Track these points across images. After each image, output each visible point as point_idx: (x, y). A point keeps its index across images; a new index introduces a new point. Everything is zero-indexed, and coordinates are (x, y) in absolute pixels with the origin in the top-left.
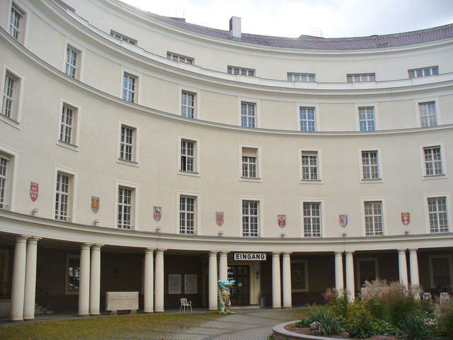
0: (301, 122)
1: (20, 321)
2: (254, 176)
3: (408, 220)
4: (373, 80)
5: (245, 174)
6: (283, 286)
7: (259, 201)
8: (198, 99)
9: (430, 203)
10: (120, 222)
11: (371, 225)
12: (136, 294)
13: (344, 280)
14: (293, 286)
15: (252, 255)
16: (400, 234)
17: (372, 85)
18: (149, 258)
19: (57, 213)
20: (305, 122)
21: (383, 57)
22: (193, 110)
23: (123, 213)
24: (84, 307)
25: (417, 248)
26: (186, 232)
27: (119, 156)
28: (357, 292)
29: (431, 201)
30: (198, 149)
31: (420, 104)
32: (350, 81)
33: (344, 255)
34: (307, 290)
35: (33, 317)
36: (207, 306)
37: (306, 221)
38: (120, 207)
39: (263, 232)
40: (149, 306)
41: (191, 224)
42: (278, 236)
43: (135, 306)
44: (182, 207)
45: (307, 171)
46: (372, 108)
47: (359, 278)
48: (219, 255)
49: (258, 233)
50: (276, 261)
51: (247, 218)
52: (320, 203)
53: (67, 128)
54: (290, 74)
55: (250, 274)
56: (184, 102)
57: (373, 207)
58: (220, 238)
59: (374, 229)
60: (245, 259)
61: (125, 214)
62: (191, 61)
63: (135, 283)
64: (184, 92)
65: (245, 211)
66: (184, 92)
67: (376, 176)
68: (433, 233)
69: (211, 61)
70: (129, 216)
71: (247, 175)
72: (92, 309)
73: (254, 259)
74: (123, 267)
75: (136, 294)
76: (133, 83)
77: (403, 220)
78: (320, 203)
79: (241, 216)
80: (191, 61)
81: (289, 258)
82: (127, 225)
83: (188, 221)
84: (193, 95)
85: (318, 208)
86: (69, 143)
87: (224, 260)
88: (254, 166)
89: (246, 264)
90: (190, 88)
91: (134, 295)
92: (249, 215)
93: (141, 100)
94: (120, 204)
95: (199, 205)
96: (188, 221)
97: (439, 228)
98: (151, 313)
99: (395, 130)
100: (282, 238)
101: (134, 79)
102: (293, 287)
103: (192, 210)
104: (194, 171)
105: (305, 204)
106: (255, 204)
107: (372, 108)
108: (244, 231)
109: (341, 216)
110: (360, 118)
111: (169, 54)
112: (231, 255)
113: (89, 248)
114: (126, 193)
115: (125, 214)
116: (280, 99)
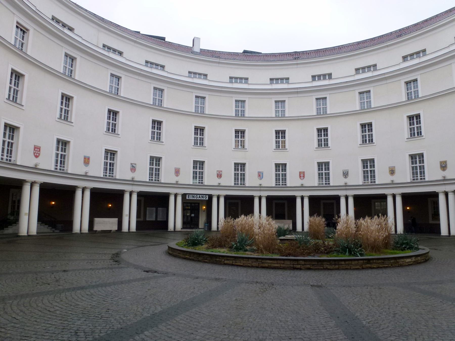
0: (195, 106)
1: (24, 236)
3: (304, 176)
4: (246, 83)
5: (153, 138)
6: (175, 218)
7: (161, 158)
10: (57, 166)
11: (279, 179)
12: (116, 220)
14: (138, 216)
15: (198, 196)
18: (79, 193)
19: (2, 155)
22: (118, 89)
23: (59, 159)
24: (76, 228)
25: (266, 195)
27: (58, 116)
30: (121, 118)
32: (231, 82)
33: (260, 198)
35: (35, 234)
38: (57, 154)
39: (247, 183)
40: (125, 228)
41: (112, 170)
43: (115, 228)
44: (106, 158)
45: (197, 140)
46: (244, 101)
48: (131, 193)
49: (159, 179)
50: (215, 200)
51: (153, 168)
53: (14, 90)
56: (111, 82)
57: (323, 166)
58: (177, 185)
59: (281, 181)
61: (61, 160)
62: (121, 53)
63: (117, 213)
65: (151, 164)
67: (326, 145)
69: (135, 56)
70: (64, 161)
72: (30, 230)
74: (106, 201)
75: (116, 220)
76: (72, 62)
77: (300, 177)
78: (204, 161)
80: (121, 53)
81: (181, 197)
82: (62, 168)
83: (110, 167)
84: (119, 78)
85: (203, 165)
86: (16, 102)
87: (179, 199)
88: (160, 133)
89: (198, 202)
90: (117, 73)
91: (115, 220)
92: (154, 167)
93: (77, 76)
94: (57, 152)
96: (110, 167)
97: (281, 183)
98: (126, 232)
99: (298, 117)
101: (73, 59)
102: (439, 225)
103: (113, 160)
104: (116, 132)
105: (235, 164)
106: (159, 160)
107: (244, 101)
108: (150, 177)
109: (259, 173)
110: (276, 108)
111: (104, 46)
112: (184, 196)
113: (30, 184)
114: (63, 144)
115: (61, 160)
116: (388, 81)
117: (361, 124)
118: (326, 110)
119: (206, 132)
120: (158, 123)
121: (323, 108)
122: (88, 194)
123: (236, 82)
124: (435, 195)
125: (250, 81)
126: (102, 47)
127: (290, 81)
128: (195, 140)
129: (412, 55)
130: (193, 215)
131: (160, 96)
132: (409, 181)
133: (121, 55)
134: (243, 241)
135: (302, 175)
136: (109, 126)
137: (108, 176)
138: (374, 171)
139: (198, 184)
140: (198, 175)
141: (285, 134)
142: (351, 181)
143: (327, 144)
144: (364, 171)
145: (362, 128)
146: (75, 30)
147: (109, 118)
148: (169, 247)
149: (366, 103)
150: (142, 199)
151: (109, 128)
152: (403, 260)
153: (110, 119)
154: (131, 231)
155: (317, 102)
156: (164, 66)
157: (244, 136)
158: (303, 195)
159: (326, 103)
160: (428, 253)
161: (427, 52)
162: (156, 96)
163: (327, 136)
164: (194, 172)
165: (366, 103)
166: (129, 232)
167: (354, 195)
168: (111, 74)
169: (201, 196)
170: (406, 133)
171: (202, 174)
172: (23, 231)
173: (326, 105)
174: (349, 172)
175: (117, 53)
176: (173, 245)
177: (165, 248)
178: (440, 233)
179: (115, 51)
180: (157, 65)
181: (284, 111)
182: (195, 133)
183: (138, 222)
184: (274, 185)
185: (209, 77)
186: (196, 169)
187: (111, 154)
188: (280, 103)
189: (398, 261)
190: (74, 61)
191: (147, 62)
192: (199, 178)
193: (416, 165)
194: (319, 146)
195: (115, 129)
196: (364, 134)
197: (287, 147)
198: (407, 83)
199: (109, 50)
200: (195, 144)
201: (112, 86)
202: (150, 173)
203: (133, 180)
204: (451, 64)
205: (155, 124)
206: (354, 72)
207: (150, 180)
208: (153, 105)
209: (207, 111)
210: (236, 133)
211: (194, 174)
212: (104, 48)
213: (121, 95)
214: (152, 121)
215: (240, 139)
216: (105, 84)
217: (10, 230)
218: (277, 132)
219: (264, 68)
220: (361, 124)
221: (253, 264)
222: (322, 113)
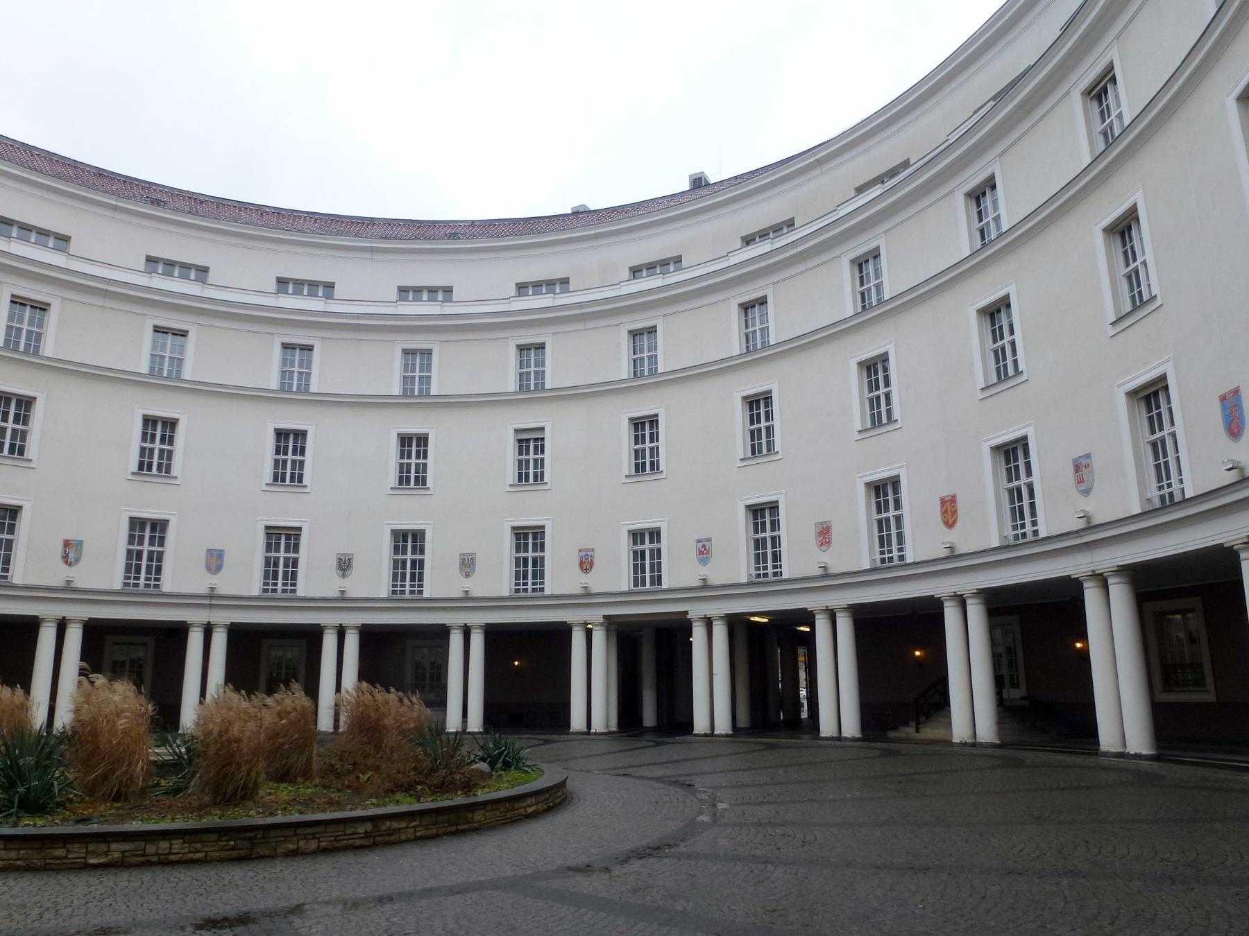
9: (132, 528)
11: (526, 573)
17: (57, 259)
21: (110, 213)
24: (700, 723)
29: (137, 524)
31: (157, 330)
33: (62, 626)
34: (1210, 697)
36: (688, 726)
37: (270, 563)
39: (303, 588)
42: (202, 589)
46: (309, 348)
48: (708, 623)
52: (21, 507)
57: (283, 539)
68: (395, 597)
83: (766, 550)
96: (766, 550)
107: (309, 348)
118: (429, 383)
119: (38, 413)
121: (420, 377)
122: (845, 625)
125: (212, 277)
127: (338, 293)
132: (506, 593)
134: (291, 754)
135: (215, 561)
137: (770, 574)
138: (422, 562)
140: (408, 571)
143: (169, 467)
149: (417, 379)
155: (284, 354)
158: (213, 620)
163: (425, 457)
166: (839, 738)
167: (487, 624)
172: (959, 730)
173: (429, 370)
174: (355, 564)
178: (1091, 732)
181: (309, 374)
184: (118, 585)
185: (73, 248)
187: (762, 514)
188: (417, 358)
193: (276, 555)
194: (275, 479)
196: (524, 457)
217: (928, 732)
222: (415, 393)
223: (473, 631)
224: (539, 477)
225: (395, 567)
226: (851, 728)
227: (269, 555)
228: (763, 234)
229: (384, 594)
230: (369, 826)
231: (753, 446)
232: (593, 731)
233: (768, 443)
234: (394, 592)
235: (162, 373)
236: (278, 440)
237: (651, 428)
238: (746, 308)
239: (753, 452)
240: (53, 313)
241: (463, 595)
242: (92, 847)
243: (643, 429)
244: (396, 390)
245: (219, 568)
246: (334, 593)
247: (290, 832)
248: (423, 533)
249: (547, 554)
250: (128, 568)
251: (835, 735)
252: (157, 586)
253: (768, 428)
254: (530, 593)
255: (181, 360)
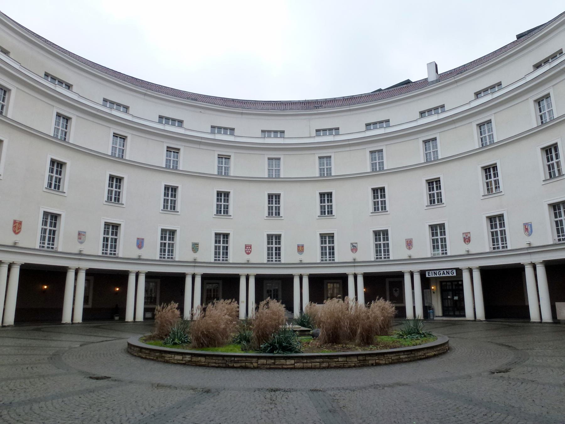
0: (167, 159)
2: (118, 201)
8: (73, 123)
11: (380, 250)
13: (193, 295)
15: (442, 272)
16: (243, 262)
20: (170, 160)
22: (66, 133)
26: (501, 248)
28: (257, 308)
33: (301, 277)
41: (52, 240)
45: (167, 203)
46: (381, 151)
47: (205, 297)
48: (77, 271)
54: (161, 117)
55: (106, 288)
56: (57, 123)
59: (383, 254)
60: (448, 275)
62: (69, 86)
64: (59, 115)
66: (59, 115)
68: (322, 262)
71: (111, 200)
73: (444, 275)
79: (102, 236)
80: (69, 86)
81: (144, 277)
83: (49, 236)
88: (119, 192)
90: (66, 112)
95: (62, 224)
97: (383, 256)
98: (69, 324)
100: (410, 258)
104: (61, 190)
108: (103, 250)
117: (372, 189)
118: (383, 165)
119: (179, 192)
120: (117, 179)
121: (379, 163)
123: (219, 133)
124: (400, 275)
125: (236, 133)
126: (43, 76)
127: (341, 132)
128: (164, 203)
129: (429, 111)
130: (456, 298)
131: (122, 144)
133: (69, 89)
136: (51, 180)
138: (388, 244)
139: (441, 255)
140: (440, 244)
141: (279, 198)
142: (360, 256)
144: (322, 248)
145: (374, 193)
146: (11, 54)
147: (52, 171)
148: (129, 344)
149: (377, 164)
150: (92, 278)
151: (51, 184)
152: (170, 356)
153: (52, 172)
154: (137, 320)
156: (129, 107)
157: (228, 200)
158: (249, 273)
159: (330, 163)
160: (447, 342)
161: (446, 108)
162: (116, 144)
163: (385, 197)
164: (161, 243)
165: (377, 164)
166: (72, 323)
168: (57, 113)
169: (445, 271)
170: (426, 200)
171: (173, 247)
175: (64, 86)
176: (135, 340)
177: (122, 344)
178: (528, 316)
179: (61, 82)
180: (119, 105)
182: (165, 193)
183: (85, 311)
186: (165, 240)
188: (274, 161)
189: (163, 355)
190: (7, 94)
191: (105, 100)
192: (442, 248)
193: (437, 237)
195: (59, 186)
197: (281, 214)
198: (425, 142)
199: (53, 81)
200: (164, 208)
201: (58, 129)
202: (104, 244)
203: (80, 254)
204: (471, 122)
205: (113, 181)
206: (364, 128)
207: (103, 253)
208: (111, 156)
209: (181, 167)
210: (218, 196)
211: (161, 246)
212: (46, 77)
213: (70, 142)
214: (110, 177)
215: (380, 199)
216: (48, 125)
218: (322, 195)
219: (336, 115)
220: (372, 189)
221: (273, 361)
222: (326, 174)
223: (304, 277)
224: (440, 201)
225: (376, 247)
226: (481, 314)
227: (433, 238)
228: (546, 61)
229: (373, 259)
230: (344, 359)
231: (550, 173)
232: (137, 320)
233: (559, 170)
234: (377, 258)
235: (274, 177)
236: (321, 197)
237: (494, 171)
238: (539, 102)
239: (551, 176)
240: (232, 158)
241: (466, 253)
242: (293, 366)
243: (490, 172)
244: (369, 169)
245: (356, 250)
246: (406, 257)
247: (244, 359)
248: (387, 231)
249: (447, 236)
250: (268, 254)
251: (473, 319)
252: (280, 261)
253: (557, 163)
254: (501, 249)
255: (279, 170)
